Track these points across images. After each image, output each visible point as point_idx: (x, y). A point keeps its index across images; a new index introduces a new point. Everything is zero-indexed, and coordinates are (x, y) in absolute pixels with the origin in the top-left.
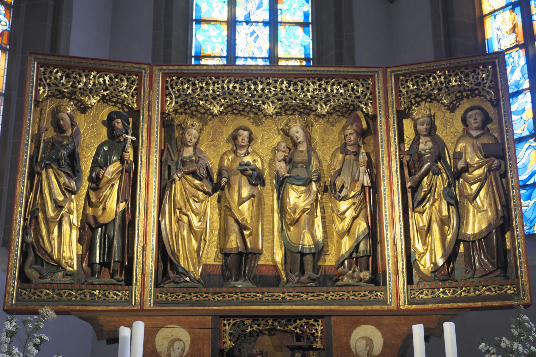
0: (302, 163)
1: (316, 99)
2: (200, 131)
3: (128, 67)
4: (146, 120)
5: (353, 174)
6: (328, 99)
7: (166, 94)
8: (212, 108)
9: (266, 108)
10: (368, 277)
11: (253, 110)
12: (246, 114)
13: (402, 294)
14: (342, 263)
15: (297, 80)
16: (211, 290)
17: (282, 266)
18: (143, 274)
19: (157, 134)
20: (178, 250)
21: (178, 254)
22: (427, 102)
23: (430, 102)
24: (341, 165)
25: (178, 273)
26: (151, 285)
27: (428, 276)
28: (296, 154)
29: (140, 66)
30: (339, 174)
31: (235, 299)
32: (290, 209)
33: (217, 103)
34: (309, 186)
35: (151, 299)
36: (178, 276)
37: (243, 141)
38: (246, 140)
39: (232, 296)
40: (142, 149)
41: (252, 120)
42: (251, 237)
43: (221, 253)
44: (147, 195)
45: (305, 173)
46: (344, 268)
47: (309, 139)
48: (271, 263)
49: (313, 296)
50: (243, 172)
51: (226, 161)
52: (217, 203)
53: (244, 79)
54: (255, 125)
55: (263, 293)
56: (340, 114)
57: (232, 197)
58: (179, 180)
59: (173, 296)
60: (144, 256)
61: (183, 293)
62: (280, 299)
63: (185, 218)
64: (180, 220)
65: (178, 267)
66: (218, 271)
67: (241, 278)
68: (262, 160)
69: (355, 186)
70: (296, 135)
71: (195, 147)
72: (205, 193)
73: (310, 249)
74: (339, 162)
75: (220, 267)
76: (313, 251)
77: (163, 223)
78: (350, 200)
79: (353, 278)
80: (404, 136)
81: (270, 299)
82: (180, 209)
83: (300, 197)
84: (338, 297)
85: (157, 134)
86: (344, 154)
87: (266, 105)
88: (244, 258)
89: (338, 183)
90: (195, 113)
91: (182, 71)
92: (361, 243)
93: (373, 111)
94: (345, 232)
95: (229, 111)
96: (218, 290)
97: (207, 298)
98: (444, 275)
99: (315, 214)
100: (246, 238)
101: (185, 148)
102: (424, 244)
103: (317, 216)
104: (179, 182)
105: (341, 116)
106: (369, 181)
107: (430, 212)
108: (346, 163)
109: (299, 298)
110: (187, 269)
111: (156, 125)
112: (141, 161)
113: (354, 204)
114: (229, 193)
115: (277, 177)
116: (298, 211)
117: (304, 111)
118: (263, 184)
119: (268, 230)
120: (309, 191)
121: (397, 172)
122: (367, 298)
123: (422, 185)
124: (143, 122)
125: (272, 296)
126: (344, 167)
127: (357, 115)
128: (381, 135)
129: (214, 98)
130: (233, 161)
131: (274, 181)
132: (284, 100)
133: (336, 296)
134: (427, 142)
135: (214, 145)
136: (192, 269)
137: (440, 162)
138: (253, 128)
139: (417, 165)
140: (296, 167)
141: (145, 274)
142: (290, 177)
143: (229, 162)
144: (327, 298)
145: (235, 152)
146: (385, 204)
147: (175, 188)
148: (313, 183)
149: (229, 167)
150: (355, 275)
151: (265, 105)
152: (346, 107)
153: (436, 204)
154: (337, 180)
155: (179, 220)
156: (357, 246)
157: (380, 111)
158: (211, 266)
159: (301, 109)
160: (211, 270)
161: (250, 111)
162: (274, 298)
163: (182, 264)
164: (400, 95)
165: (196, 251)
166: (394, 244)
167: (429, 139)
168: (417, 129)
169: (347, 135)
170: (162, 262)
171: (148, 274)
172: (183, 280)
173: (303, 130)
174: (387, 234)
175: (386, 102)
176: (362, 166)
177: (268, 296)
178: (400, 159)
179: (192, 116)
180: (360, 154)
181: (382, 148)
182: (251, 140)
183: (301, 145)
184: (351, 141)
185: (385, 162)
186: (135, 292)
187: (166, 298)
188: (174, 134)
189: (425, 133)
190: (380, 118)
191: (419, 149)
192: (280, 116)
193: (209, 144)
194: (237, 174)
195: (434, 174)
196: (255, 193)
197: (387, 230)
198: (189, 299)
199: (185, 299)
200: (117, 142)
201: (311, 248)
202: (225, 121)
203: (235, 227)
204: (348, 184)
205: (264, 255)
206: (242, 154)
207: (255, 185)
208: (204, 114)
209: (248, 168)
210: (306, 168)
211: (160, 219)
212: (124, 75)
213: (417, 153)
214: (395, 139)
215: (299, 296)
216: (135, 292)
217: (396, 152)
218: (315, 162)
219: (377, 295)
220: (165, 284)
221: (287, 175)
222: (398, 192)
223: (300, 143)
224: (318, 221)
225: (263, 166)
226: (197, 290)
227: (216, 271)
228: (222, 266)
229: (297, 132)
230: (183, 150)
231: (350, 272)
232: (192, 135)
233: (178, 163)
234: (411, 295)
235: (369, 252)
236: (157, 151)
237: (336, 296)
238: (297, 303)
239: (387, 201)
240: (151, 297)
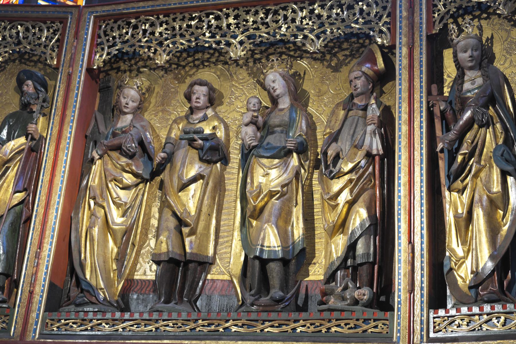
0: (279, 126)
3: (49, 12)
6: (322, 29)
7: (96, 45)
13: (419, 324)
15: (277, 7)
22: (482, 19)
23: (486, 19)
29: (66, 10)
33: (164, 51)
34: (285, 158)
35: (36, 329)
37: (198, 100)
42: (193, 237)
49: (272, 326)
50: (191, 142)
53: (203, 14)
56: (348, 53)
70: (272, 85)
74: (338, 122)
75: (152, 283)
80: (443, 75)
81: (206, 329)
84: (312, 328)
91: (120, 12)
92: (359, 242)
98: (494, 292)
105: (350, 56)
106: (380, 147)
110: (93, 283)
117: (295, 53)
118: (225, 160)
119: (226, 228)
122: (360, 330)
125: (209, 325)
129: (161, 44)
137: (494, 107)
140: (273, 133)
144: (294, 329)
150: (348, 295)
153: (483, 175)
157: (400, 38)
159: (290, 51)
163: (88, 276)
164: (433, 11)
168: (457, 60)
175: (411, 26)
176: (370, 125)
177: (203, 326)
181: (400, 93)
184: (358, 88)
189: (470, 64)
195: (480, 127)
200: (28, 112)
205: (218, 265)
206: (196, 120)
207: (209, 162)
212: (45, 23)
213: (460, 97)
214: (421, 78)
215: (249, 326)
225: (227, 135)
236: (73, 120)
237: (309, 328)
238: (246, 337)
240: (37, 326)
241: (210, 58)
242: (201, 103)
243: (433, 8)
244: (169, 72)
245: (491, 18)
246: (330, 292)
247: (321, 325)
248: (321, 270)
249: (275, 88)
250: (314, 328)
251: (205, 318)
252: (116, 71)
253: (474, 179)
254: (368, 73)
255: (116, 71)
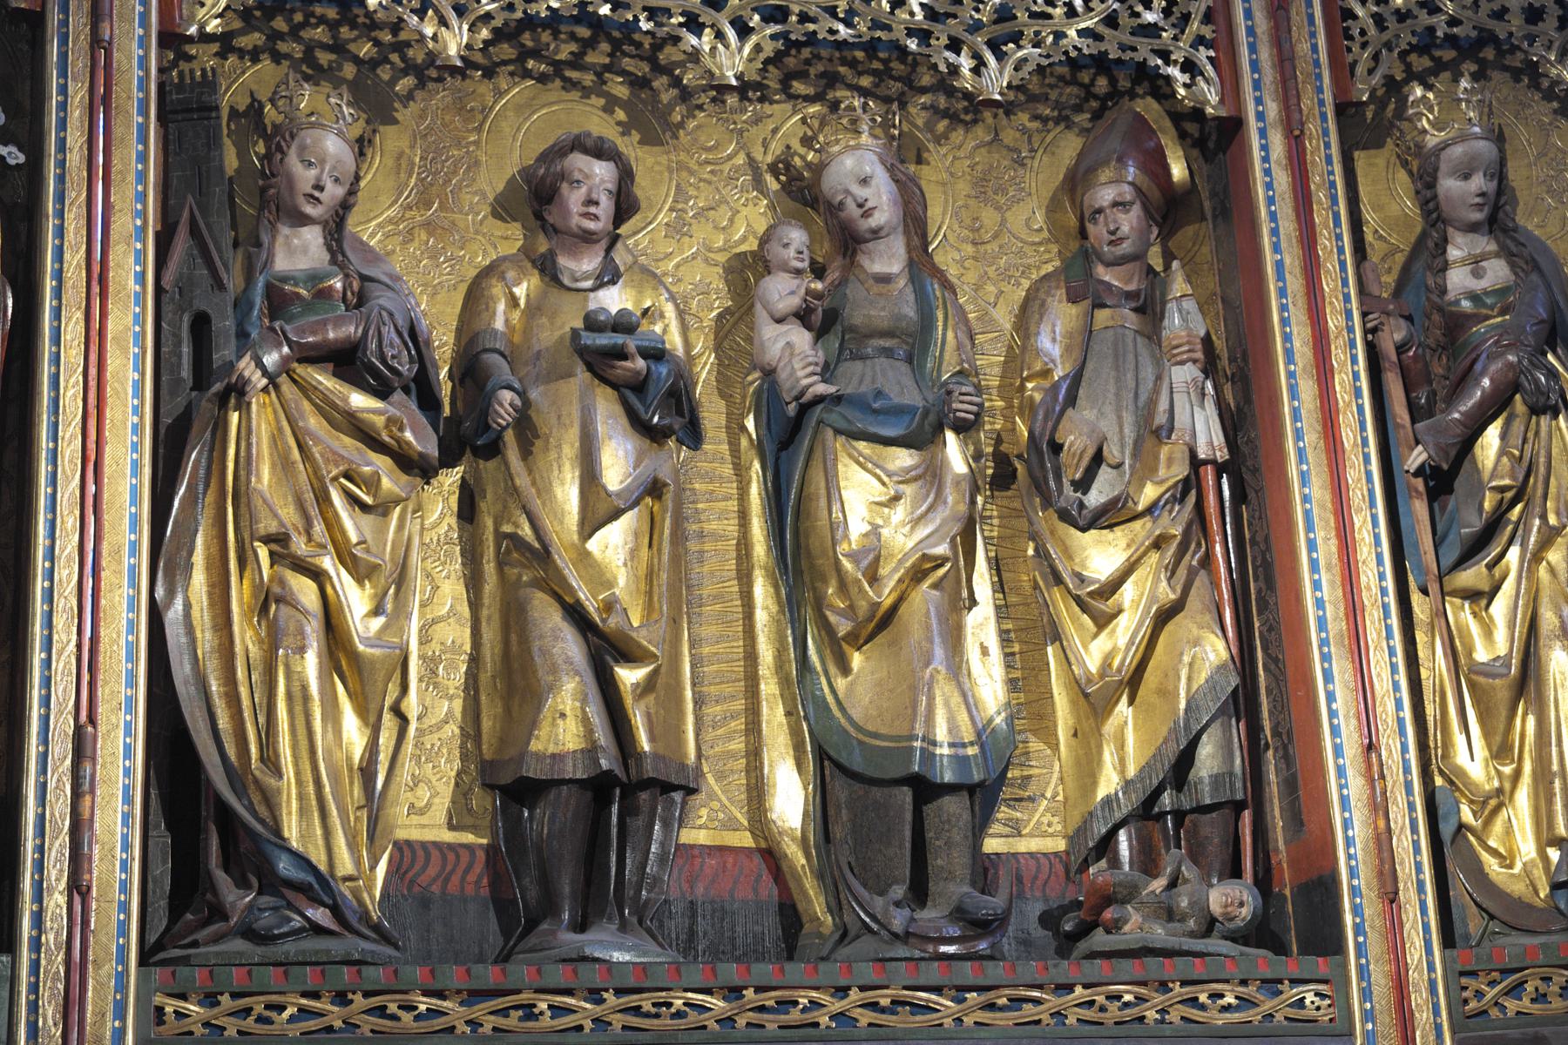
1: (952, 22)
2: (362, 146)
4: (79, 63)
5: (1143, 398)
6: (1007, 27)
8: (429, 31)
9: (707, 48)
10: (1246, 912)
11: (628, 63)
12: (588, 79)
14: (1106, 845)
16: (453, 976)
17: (807, 855)
18: (77, 887)
19: (144, 139)
20: (271, 761)
21: (272, 782)
24: (1077, 354)
25: (270, 883)
26: (123, 951)
27: (1530, 907)
28: (854, 291)
30: (1071, 400)
31: (588, 1025)
32: (853, 556)
34: (932, 448)
36: (266, 900)
37: (593, 210)
38: (605, 207)
39: (569, 1011)
40: (60, 214)
41: (621, 115)
42: (651, 698)
43: (489, 786)
44: (93, 464)
45: (908, 381)
46: (1115, 863)
47: (915, 223)
48: (746, 840)
49: (991, 1007)
51: (501, 307)
52: (453, 521)
54: (636, 136)
55: (734, 992)
57: (545, 490)
58: (265, 390)
59: (247, 1011)
60: (86, 787)
61: (304, 995)
62: (824, 1020)
63: (305, 590)
64: (278, 601)
65: (269, 849)
66: (471, 878)
67: (601, 913)
68: (681, 314)
69: (1156, 458)
70: (861, 192)
71: (336, 228)
72: (406, 462)
73: (961, 762)
75: (481, 855)
76: (977, 777)
77: (173, 615)
78: (1137, 525)
79: (1170, 914)
82: (278, 541)
83: (896, 498)
85: (144, 139)
86: (1087, 303)
87: (705, 39)
88: (615, 809)
89: (1075, 440)
90: (324, 58)
92: (1204, 737)
93: (1222, 101)
94: (1121, 682)
95: (505, 63)
96: (489, 975)
97: (439, 1023)
99: (965, 594)
100: (628, 700)
101: (285, 230)
102: (1501, 750)
103: (973, 602)
104: (263, 397)
105: (1057, 122)
106: (1218, 438)
107: (1528, 590)
108: (1102, 346)
109: (919, 1018)
110: (319, 858)
111: (137, 94)
112: (59, 275)
113: (1158, 544)
114: (530, 472)
115: (769, 397)
116: (891, 577)
117: (877, 85)
118: (693, 435)
120: (932, 474)
121: (1358, 393)
123: (1474, 462)
124: (63, 73)
126: (1090, 366)
127: (1139, 118)
128: (1273, 217)
130: (534, 309)
131: (750, 423)
132: (794, 18)
133: (1103, 1009)
134: (1484, 257)
135: (428, 225)
136: (345, 865)
138: (629, 147)
139: (1438, 369)
141: (89, 888)
142: (837, 399)
143: (516, 316)
145: (547, 269)
146: (1312, 546)
147: (246, 430)
148: (950, 436)
149: (517, 339)
151: (699, 36)
152: (1074, 82)
154: (1064, 424)
155: (268, 601)
156: (1186, 759)
157: (1259, 101)
158: (435, 853)
159: (860, 74)
160: (432, 871)
161: (608, 68)
162: (795, 1016)
163: (292, 831)
164: (1348, 28)
165: (361, 769)
166: (1371, 747)
167: (1493, 247)
169: (1100, 211)
170: (169, 827)
171: (105, 887)
172: (297, 921)
173: (891, 170)
174: (1331, 697)
175: (1285, 60)
176: (1182, 363)
177: (762, 1009)
178: (1366, 332)
179: (315, 73)
180: (1172, 307)
182: (625, 207)
183: (881, 245)
184: (1121, 240)
185: (1297, 344)
186: (34, 988)
187: (206, 1024)
188: (221, 160)
189: (1477, 216)
190: (1263, 133)
191: (1443, 291)
192: (762, 100)
193: (402, 219)
194: (570, 375)
195: (1535, 411)
196: (665, 474)
197: (1328, 677)
198: (338, 1024)
199: (313, 1024)
201: (967, 758)
202: (485, 111)
203: (569, 646)
204: (1122, 446)
205: (712, 796)
206: (586, 279)
208: (374, 64)
209: (631, 344)
210: (909, 360)
211: (160, 593)
213: (1440, 310)
214: (1339, 237)
216: (34, 988)
217: (1347, 298)
218: (950, 335)
219: (1300, 1003)
220: (195, 944)
221: (822, 388)
222: (1371, 492)
223: (876, 233)
224: (981, 624)
226: (376, 975)
227: (463, 879)
228: (491, 851)
229: (864, 181)
230: (274, 238)
231: (1158, 885)
232: (322, 162)
233: (251, 306)
234: (1466, 1002)
235: (1239, 785)
239: (1320, 535)
240: (123, 1019)
241: (582, 54)
242: (603, 218)
243: (1344, 20)
244: (431, 85)
245: (1491, 79)
246: (1125, 892)
247: (1140, 999)
248: (1056, 819)
249: (869, 205)
250: (1120, 1009)
251: (764, 983)
252: (215, 47)
253: (1533, 565)
254: (1149, 194)
255: (215, 47)
